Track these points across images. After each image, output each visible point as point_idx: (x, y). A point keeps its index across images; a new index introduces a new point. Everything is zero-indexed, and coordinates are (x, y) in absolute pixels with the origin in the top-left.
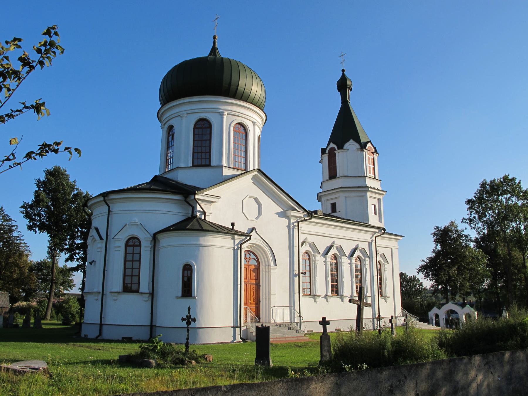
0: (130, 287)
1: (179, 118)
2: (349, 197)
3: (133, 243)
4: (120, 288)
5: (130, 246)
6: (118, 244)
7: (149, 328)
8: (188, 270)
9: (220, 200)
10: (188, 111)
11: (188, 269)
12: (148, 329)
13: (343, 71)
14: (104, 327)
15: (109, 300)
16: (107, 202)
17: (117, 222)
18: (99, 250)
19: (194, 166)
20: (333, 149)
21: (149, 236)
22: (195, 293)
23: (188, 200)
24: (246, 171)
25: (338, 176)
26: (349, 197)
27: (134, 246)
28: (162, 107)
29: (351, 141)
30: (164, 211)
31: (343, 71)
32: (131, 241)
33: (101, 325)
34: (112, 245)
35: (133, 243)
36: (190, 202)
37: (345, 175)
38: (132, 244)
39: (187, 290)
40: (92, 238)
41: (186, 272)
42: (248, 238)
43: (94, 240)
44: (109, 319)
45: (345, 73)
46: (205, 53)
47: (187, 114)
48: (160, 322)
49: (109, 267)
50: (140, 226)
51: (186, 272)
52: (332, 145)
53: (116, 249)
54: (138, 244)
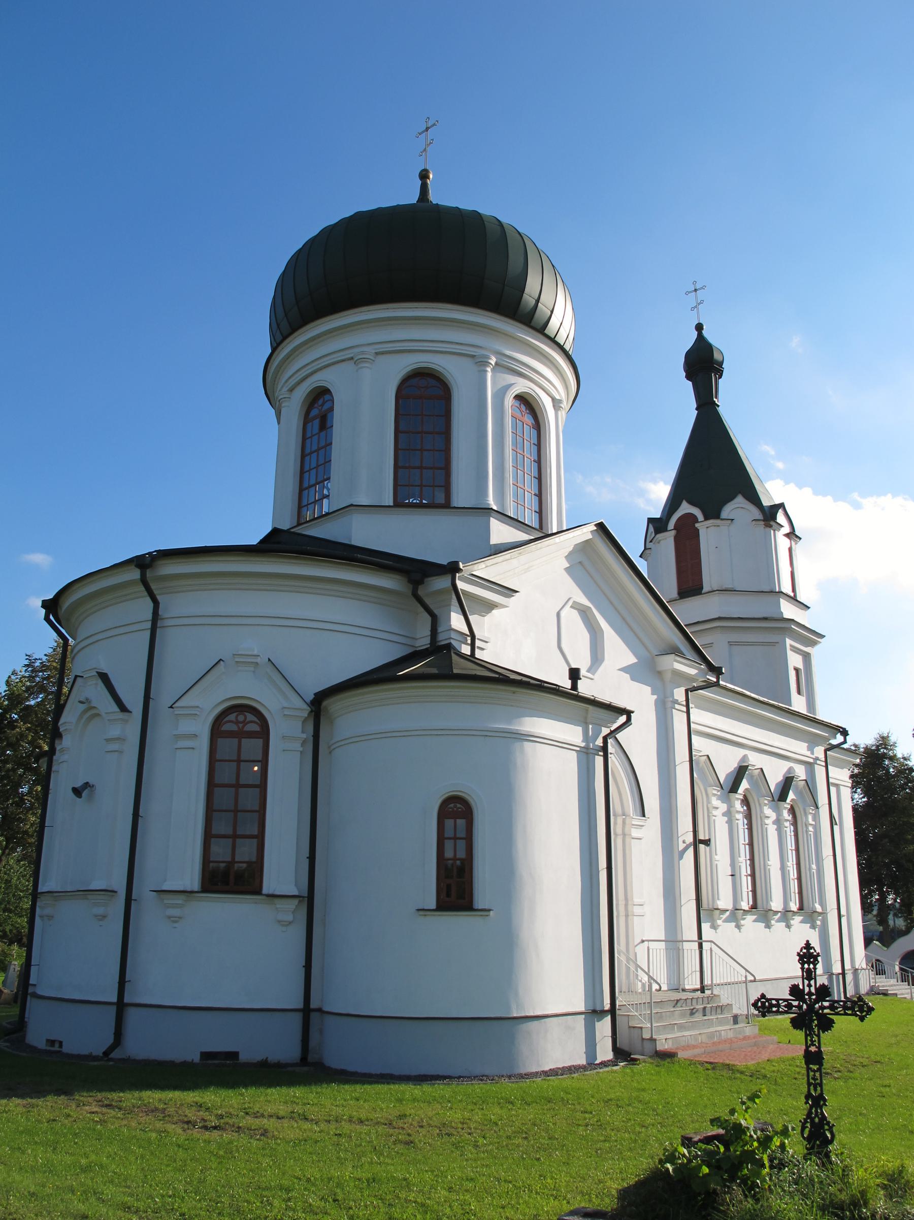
0: (234, 876)
1: (350, 366)
2: (737, 643)
3: (240, 727)
4: (191, 878)
5: (230, 734)
6: (186, 726)
7: (298, 1018)
8: (455, 816)
9: (514, 600)
10: (369, 357)
11: (456, 812)
12: (296, 1021)
13: (699, 327)
14: (132, 1015)
15: (151, 918)
16: (153, 586)
17: (183, 653)
18: (115, 746)
19: (398, 504)
20: (689, 519)
21: (305, 706)
22: (482, 896)
23: (421, 592)
24: (542, 533)
25: (705, 590)
26: (737, 643)
27: (240, 735)
28: (274, 350)
29: (740, 500)
30: (333, 629)
31: (699, 327)
32: (232, 717)
33: (121, 1006)
34: (163, 729)
35: (240, 727)
36: (428, 601)
37: (730, 586)
38: (234, 728)
39: (456, 888)
40: (83, 707)
41: (449, 823)
42: (623, 719)
43: (90, 712)
44: (155, 983)
45: (705, 333)
46: (412, 197)
47: (377, 354)
48: (335, 997)
49: (152, 808)
50: (269, 669)
51: (449, 823)
52: (686, 508)
53: (181, 744)
54: (255, 728)
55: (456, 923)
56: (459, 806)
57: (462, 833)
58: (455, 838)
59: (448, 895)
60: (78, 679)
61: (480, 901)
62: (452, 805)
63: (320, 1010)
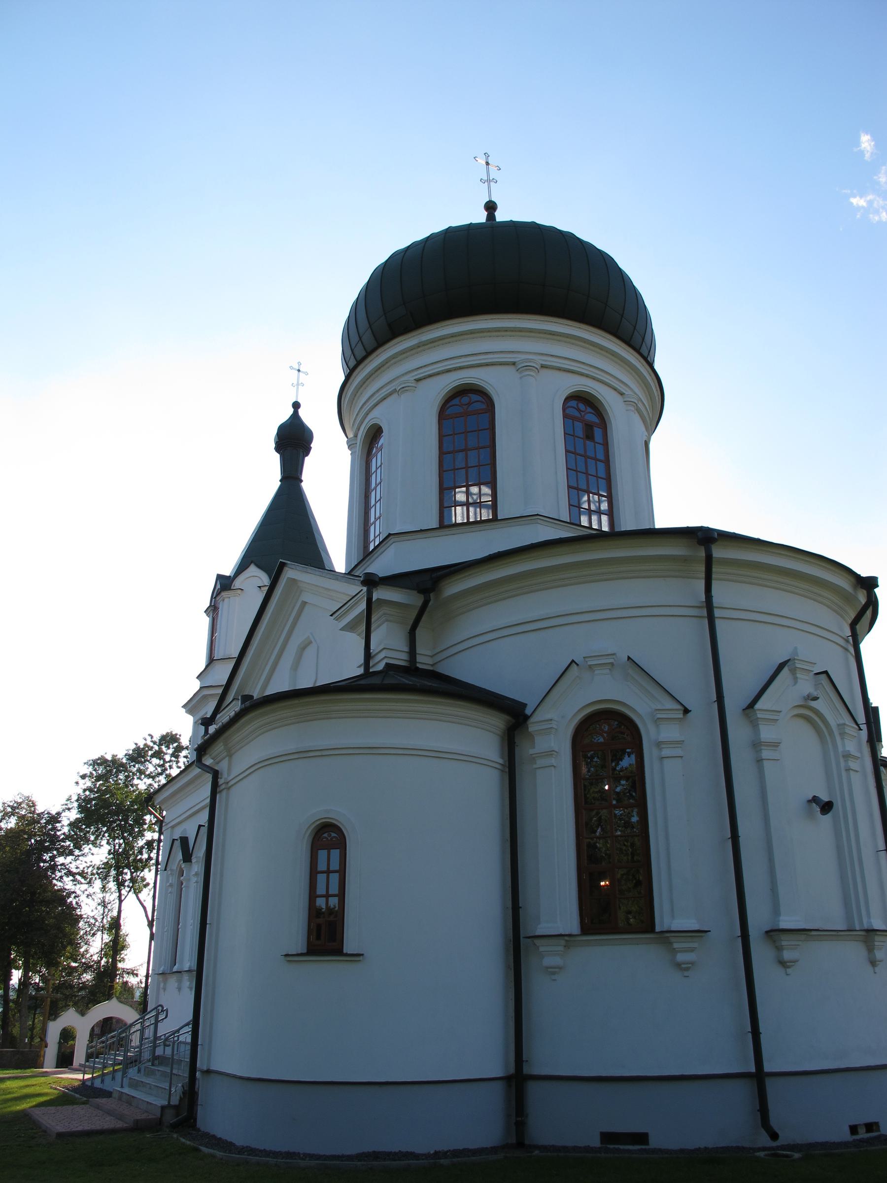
8: (329, 847)
13: (296, 406)
14: (771, 1086)
31: (296, 406)
45: (301, 412)
55: (325, 970)
56: (333, 835)
57: (335, 865)
58: (328, 872)
59: (318, 937)
60: (574, 665)
61: (349, 946)
62: (326, 835)
63: (208, 1072)
